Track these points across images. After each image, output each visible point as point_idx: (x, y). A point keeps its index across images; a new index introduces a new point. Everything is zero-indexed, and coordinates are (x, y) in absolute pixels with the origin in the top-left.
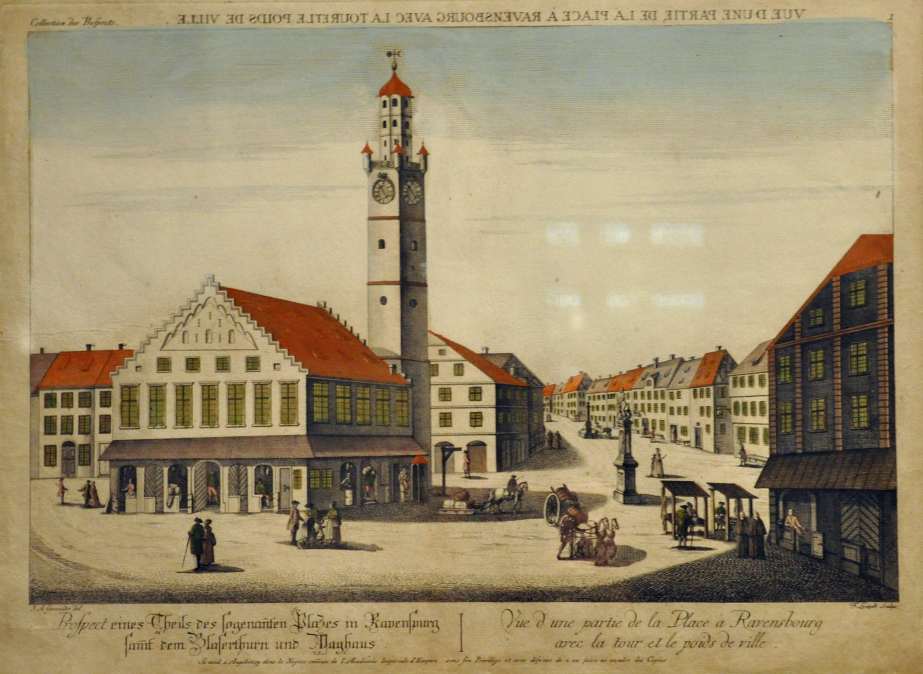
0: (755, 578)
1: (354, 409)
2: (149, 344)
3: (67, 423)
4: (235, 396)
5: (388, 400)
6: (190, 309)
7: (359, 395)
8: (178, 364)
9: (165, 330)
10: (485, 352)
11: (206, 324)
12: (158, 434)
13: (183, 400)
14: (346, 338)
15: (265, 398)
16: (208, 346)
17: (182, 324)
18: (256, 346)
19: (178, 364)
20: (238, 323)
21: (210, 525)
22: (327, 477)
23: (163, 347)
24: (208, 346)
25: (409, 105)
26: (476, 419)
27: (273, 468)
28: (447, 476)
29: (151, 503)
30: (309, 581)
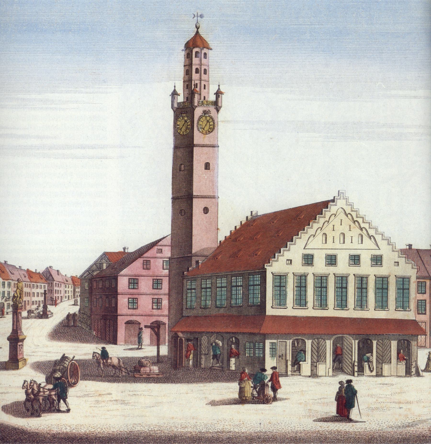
0: (10, 431)
1: (229, 294)
2: (389, 244)
3: (422, 305)
4: (321, 285)
5: (202, 288)
6: (357, 217)
7: (219, 285)
8: (366, 259)
9: (376, 234)
10: (123, 250)
11: (340, 229)
12: (382, 315)
13: (300, 287)
14: (235, 240)
15: (340, 288)
16: (344, 246)
17: (320, 229)
18: (379, 248)
19: (366, 259)
20: (364, 228)
21: (340, 386)
22: (250, 348)
23: (305, 247)
24: (344, 246)
25: (185, 71)
26: (157, 303)
27: (306, 341)
28: (160, 347)
29: (402, 367)
30: (228, 428)
